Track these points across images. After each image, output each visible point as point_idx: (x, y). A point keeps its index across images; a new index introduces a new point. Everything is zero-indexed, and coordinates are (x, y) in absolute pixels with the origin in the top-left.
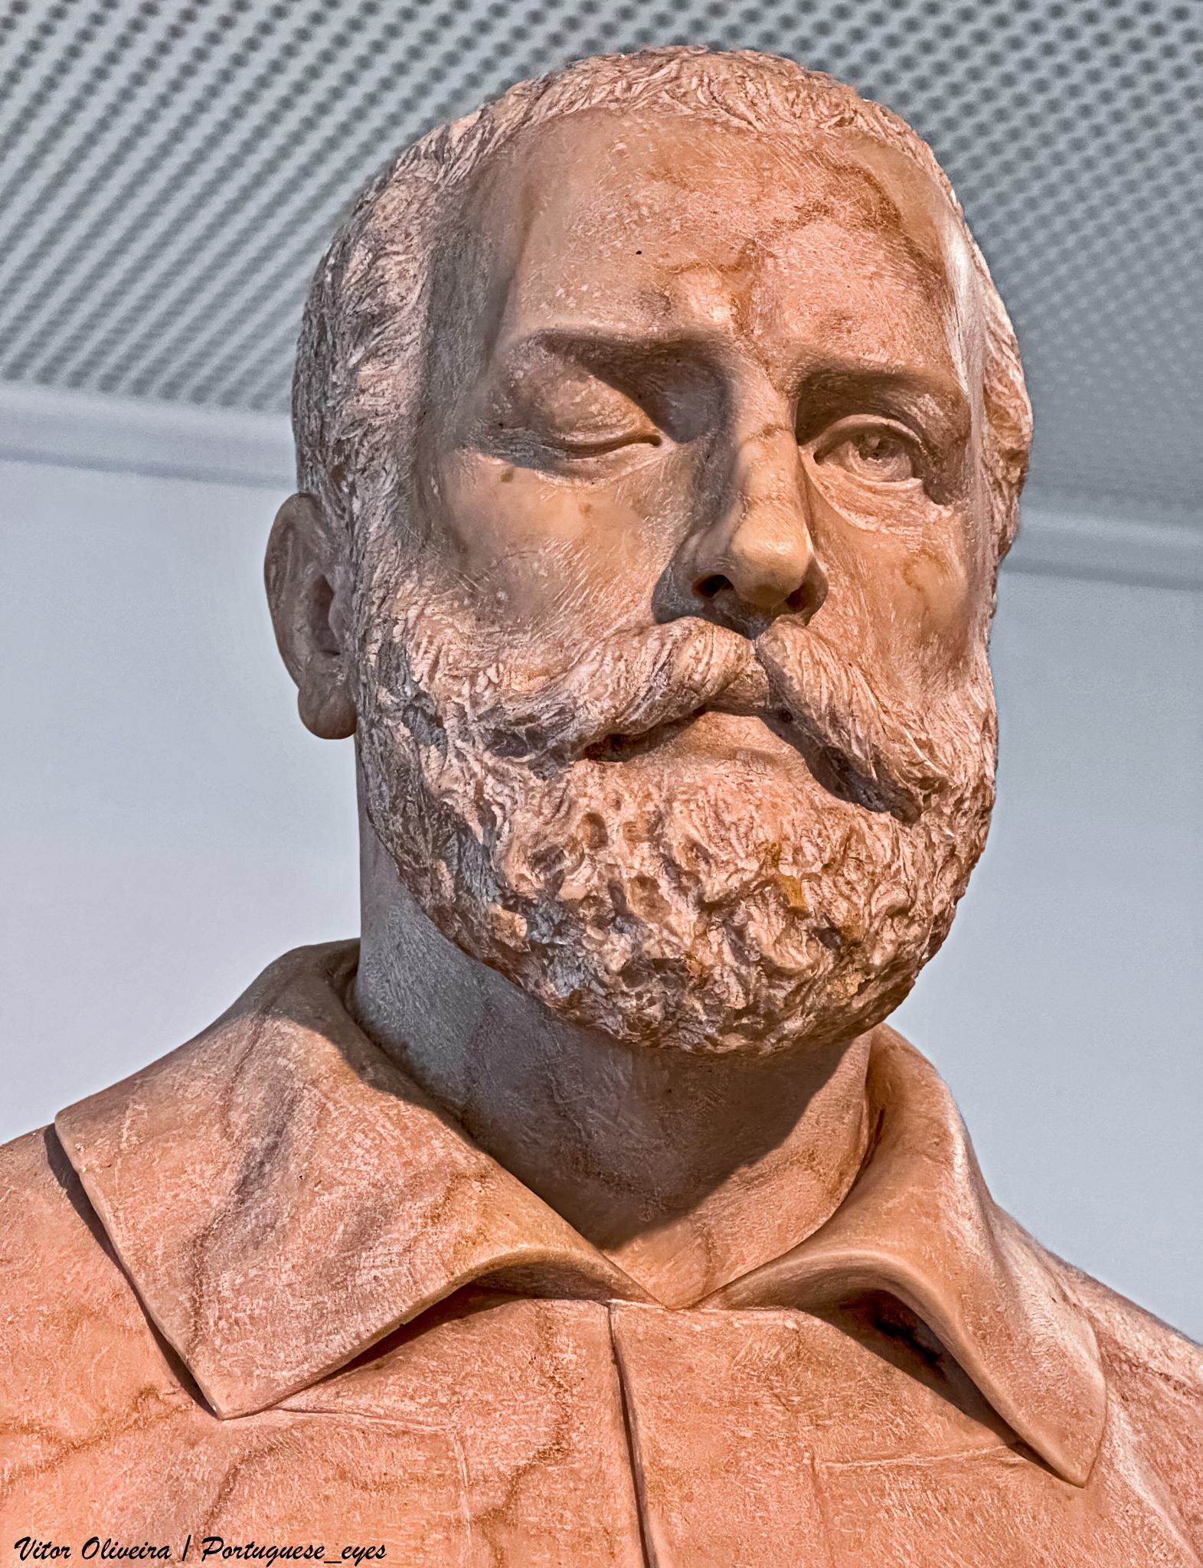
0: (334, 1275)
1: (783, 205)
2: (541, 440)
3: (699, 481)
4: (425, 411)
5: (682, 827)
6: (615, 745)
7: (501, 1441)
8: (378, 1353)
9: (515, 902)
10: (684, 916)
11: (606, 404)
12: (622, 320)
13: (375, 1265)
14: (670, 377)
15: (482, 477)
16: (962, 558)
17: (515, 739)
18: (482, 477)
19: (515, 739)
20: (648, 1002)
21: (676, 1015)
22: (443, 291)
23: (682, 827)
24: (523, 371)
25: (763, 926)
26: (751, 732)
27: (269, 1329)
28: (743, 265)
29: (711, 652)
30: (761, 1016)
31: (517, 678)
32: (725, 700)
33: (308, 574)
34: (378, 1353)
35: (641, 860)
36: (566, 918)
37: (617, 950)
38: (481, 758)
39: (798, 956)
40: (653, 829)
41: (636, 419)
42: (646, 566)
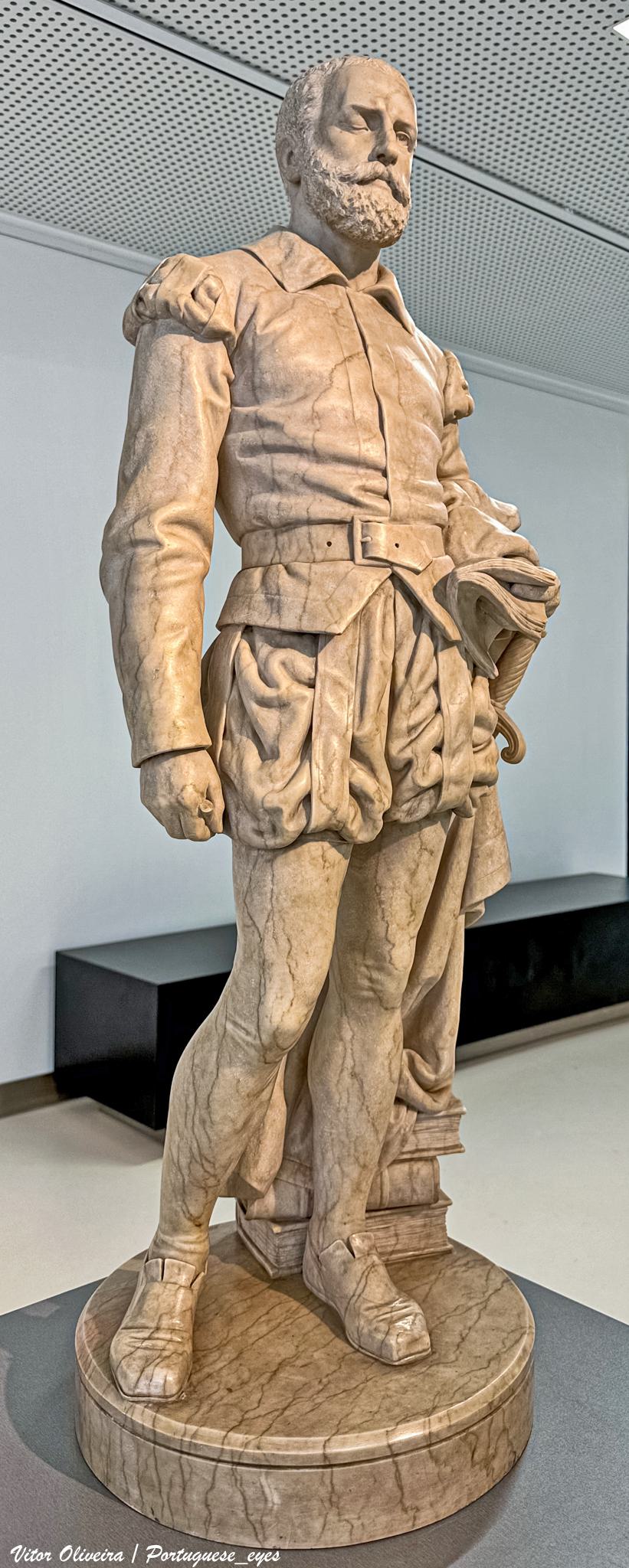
0: (306, 271)
1: (393, 89)
2: (347, 125)
3: (377, 137)
4: (322, 119)
5: (374, 198)
6: (362, 182)
7: (334, 303)
8: (311, 287)
9: (344, 207)
10: (373, 213)
11: (359, 121)
12: (367, 104)
13: (313, 271)
14: (373, 117)
15: (335, 132)
16: (190, 385)
17: (343, 179)
18: (335, 132)
19: (343, 179)
20: (365, 228)
21: (369, 231)
22: (327, 96)
23: (374, 198)
24: (347, 111)
25: (385, 217)
26: (384, 184)
27: (295, 282)
28: (387, 99)
29: (380, 168)
30: (382, 234)
31: (345, 168)
32: (380, 177)
33: (287, 151)
34: (311, 287)
35: (366, 202)
36: (353, 210)
37: (362, 218)
38: (338, 182)
39: (390, 224)
40: (369, 197)
41: (365, 125)
42: (367, 152)
